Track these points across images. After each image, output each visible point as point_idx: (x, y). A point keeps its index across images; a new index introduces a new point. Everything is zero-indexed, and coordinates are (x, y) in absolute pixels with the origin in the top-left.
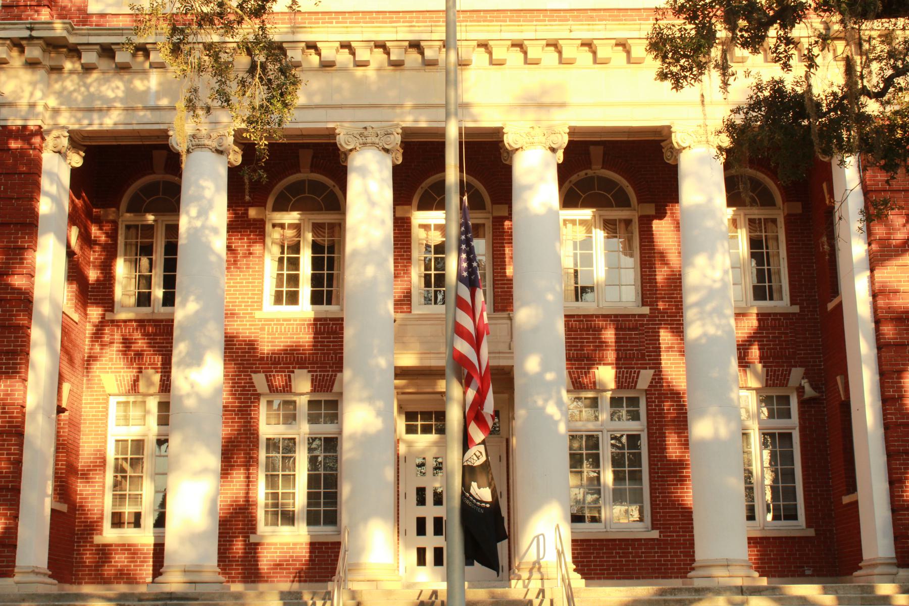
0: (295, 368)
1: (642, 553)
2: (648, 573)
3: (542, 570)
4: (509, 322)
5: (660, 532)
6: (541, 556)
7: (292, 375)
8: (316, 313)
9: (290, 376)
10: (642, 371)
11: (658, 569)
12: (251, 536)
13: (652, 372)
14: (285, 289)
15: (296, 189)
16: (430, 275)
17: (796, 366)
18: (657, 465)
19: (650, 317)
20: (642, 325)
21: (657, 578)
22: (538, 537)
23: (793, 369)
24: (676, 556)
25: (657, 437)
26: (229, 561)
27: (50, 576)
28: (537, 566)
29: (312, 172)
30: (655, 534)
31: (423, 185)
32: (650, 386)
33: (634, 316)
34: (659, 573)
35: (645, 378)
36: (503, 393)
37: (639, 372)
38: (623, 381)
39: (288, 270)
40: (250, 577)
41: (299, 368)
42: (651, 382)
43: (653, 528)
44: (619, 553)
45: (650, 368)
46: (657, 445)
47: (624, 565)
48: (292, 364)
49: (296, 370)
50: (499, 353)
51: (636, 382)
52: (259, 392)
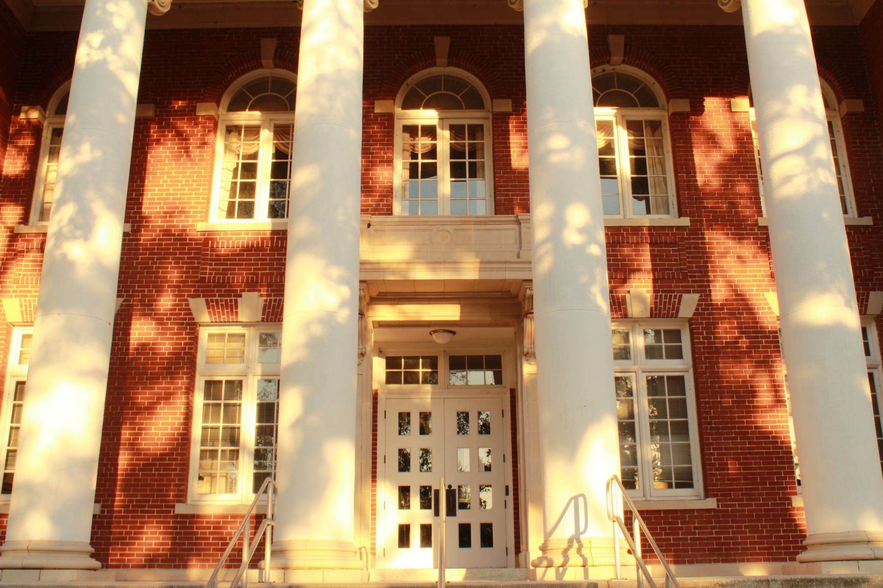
0: (244, 291)
1: (695, 528)
2: (705, 555)
3: (583, 551)
4: (516, 227)
5: (718, 501)
6: (582, 529)
7: (239, 299)
8: (273, 224)
9: (236, 301)
10: (685, 296)
11: (716, 550)
12: (178, 505)
13: (697, 296)
14: (237, 200)
15: (256, 87)
16: (417, 163)
17: (874, 290)
18: (709, 413)
19: (690, 230)
20: (682, 239)
21: (716, 561)
22: (575, 498)
23: (872, 293)
24: (741, 533)
25: (707, 378)
26: (197, 539)
27: (92, 556)
28: (576, 545)
29: (276, 66)
30: (711, 503)
31: (409, 81)
32: (695, 314)
33: (671, 228)
34: (718, 555)
35: (689, 304)
36: (506, 325)
37: (680, 297)
38: (663, 308)
39: (242, 177)
40: (174, 561)
41: (248, 291)
42: (697, 309)
43: (707, 496)
44: (665, 529)
45: (695, 292)
46: (708, 387)
47: (672, 545)
48: (240, 286)
49: (243, 293)
50: (505, 262)
51: (678, 309)
52: (196, 321)
